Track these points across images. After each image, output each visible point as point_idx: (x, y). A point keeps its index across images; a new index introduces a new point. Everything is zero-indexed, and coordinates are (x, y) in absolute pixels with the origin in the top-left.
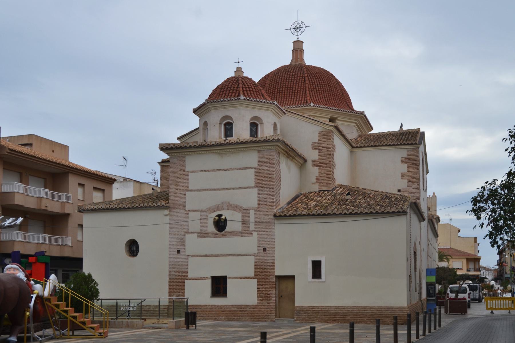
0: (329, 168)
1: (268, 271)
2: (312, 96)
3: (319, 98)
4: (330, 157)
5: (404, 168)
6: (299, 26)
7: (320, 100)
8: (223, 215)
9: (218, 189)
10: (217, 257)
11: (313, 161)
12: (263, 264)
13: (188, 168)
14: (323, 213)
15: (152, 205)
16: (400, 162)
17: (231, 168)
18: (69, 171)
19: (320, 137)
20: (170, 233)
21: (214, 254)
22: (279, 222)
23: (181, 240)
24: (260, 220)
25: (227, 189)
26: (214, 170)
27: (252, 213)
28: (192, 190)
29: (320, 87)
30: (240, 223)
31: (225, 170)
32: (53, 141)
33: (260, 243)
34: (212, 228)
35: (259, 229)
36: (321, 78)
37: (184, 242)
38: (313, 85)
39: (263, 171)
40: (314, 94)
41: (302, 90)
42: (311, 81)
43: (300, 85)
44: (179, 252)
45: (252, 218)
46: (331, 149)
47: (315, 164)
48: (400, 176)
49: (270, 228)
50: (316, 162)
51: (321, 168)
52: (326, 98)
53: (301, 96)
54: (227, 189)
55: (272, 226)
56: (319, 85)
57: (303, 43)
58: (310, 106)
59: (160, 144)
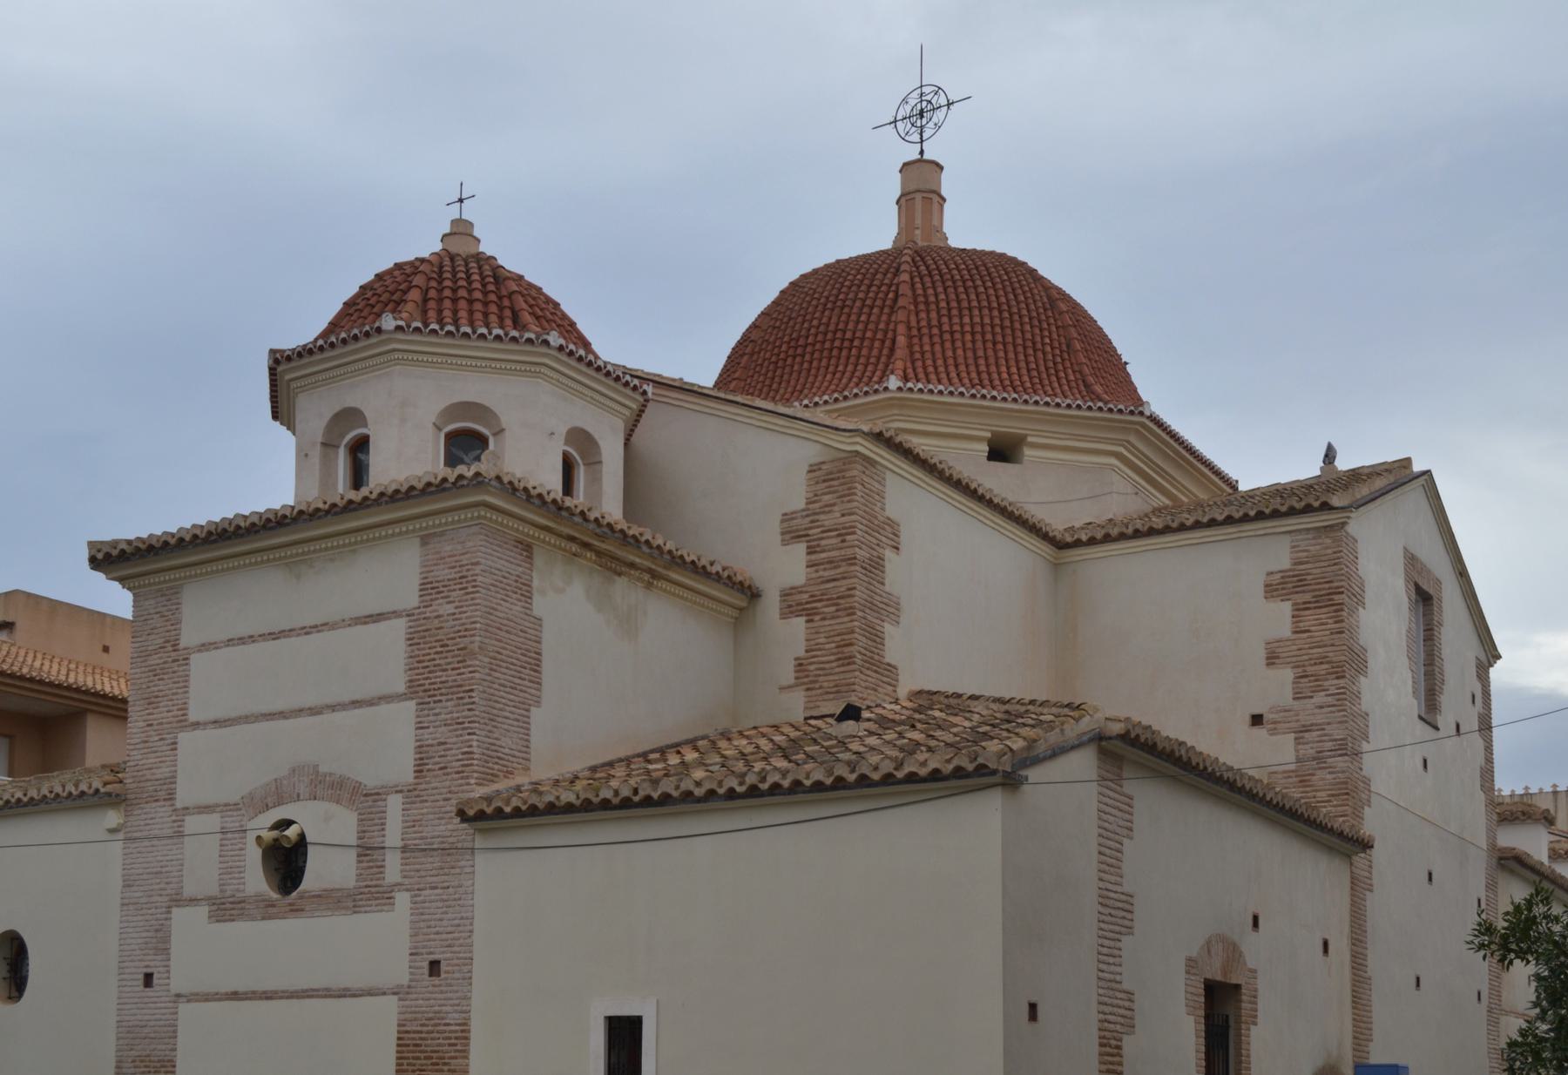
0: (846, 619)
1: (445, 1064)
2: (918, 356)
3: (951, 361)
4: (853, 568)
5: (1278, 618)
6: (924, 104)
7: (952, 368)
8: (293, 822)
9: (282, 715)
10: (270, 1002)
11: (786, 594)
12: (428, 1032)
13: (188, 638)
14: (642, 793)
15: (64, 791)
16: (1262, 593)
17: (326, 621)
18: (83, 705)
19: (814, 488)
20: (123, 905)
21: (260, 987)
22: (493, 842)
23: (157, 931)
24: (421, 838)
25: (314, 711)
26: (270, 634)
27: (395, 804)
28: (196, 725)
29: (961, 317)
30: (352, 855)
31: (307, 631)
32: (104, 615)
33: (421, 937)
34: (256, 880)
35: (417, 879)
36: (970, 283)
37: (166, 939)
38: (928, 312)
39: (436, 621)
40: (927, 348)
41: (879, 336)
42: (921, 299)
43: (873, 318)
44: (148, 979)
45: (393, 835)
46: (854, 533)
47: (793, 604)
48: (1262, 654)
49: (458, 871)
50: (797, 597)
51: (817, 618)
52: (982, 362)
53: (872, 360)
54: (314, 711)
55: (463, 863)
56: (955, 312)
57: (942, 168)
58: (886, 389)
59: (91, 544)
